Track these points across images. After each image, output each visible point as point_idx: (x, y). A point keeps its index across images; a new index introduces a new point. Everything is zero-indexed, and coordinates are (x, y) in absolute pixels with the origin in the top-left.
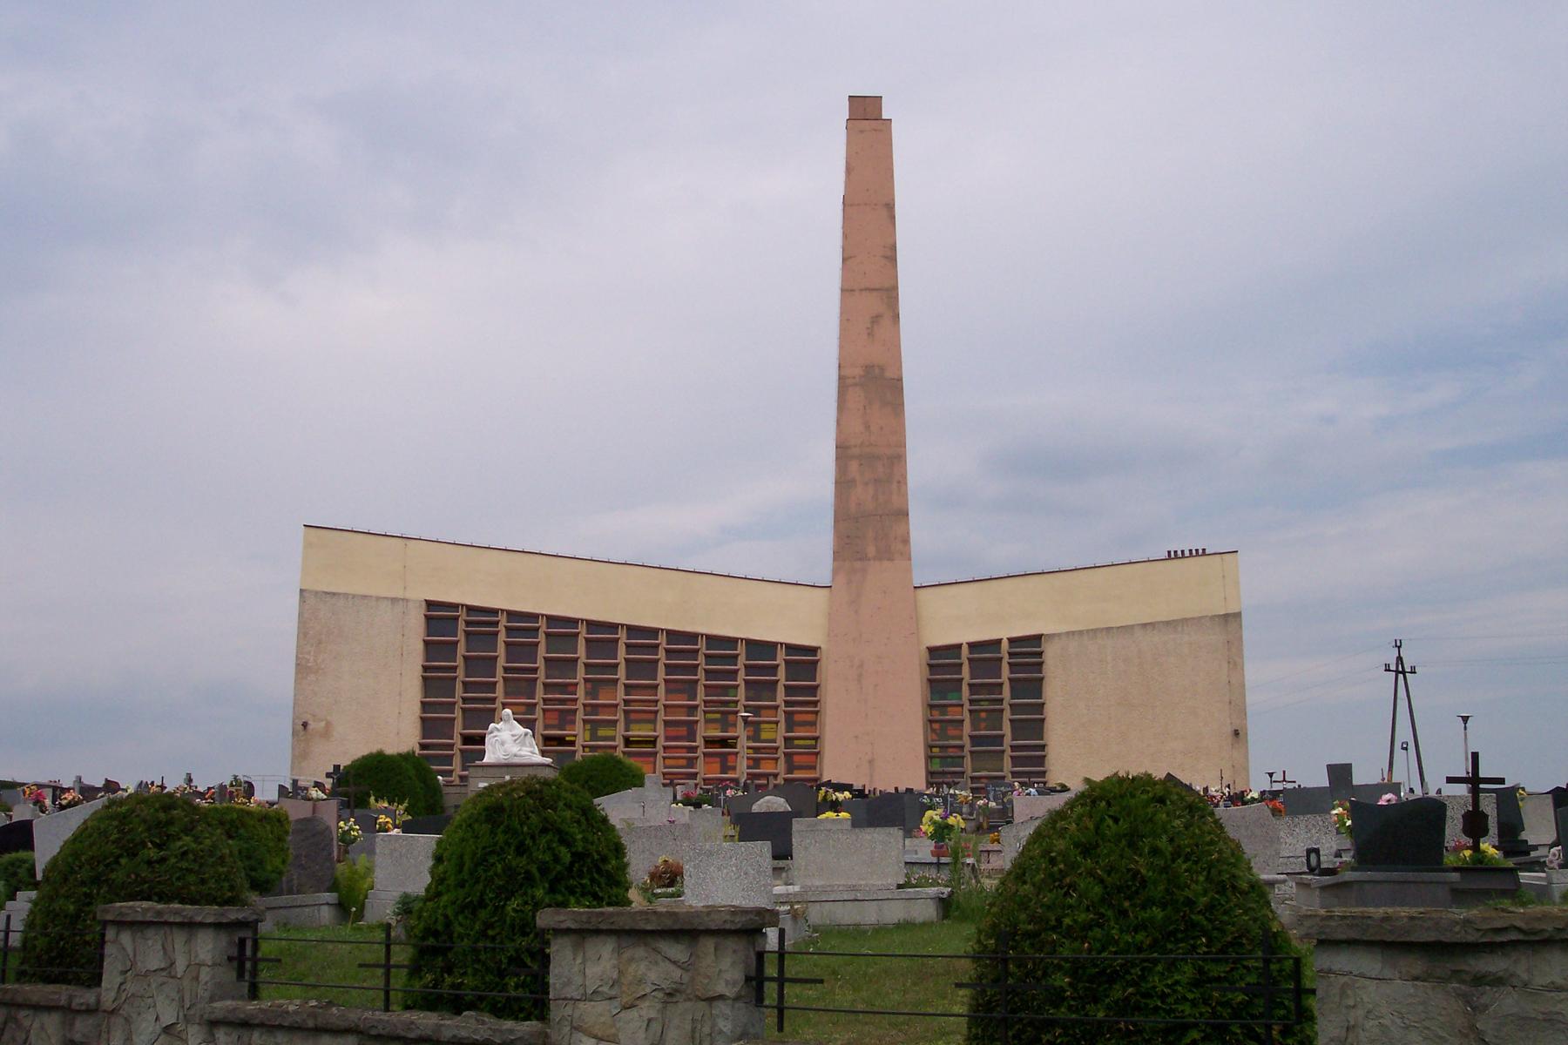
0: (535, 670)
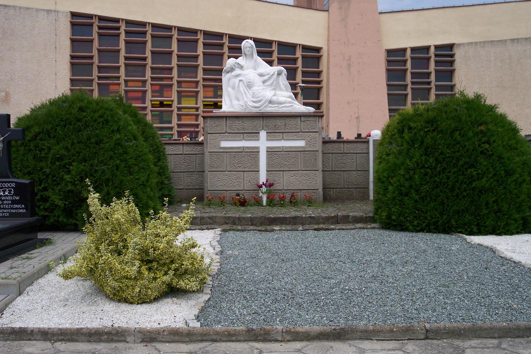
0: (91, 57)
